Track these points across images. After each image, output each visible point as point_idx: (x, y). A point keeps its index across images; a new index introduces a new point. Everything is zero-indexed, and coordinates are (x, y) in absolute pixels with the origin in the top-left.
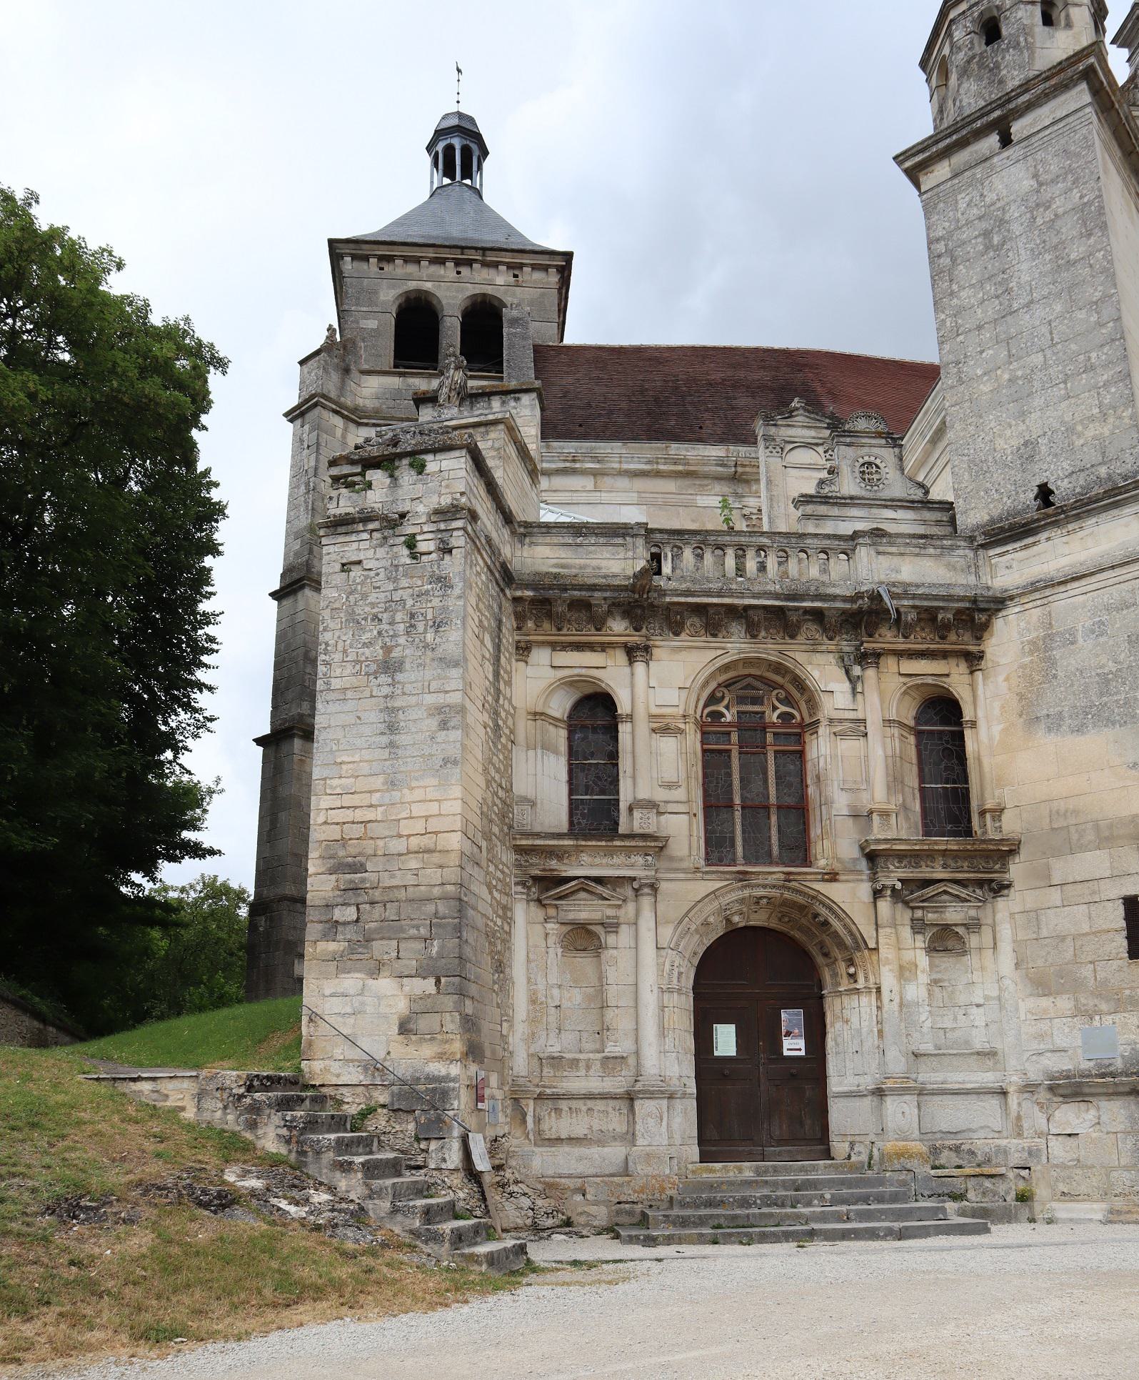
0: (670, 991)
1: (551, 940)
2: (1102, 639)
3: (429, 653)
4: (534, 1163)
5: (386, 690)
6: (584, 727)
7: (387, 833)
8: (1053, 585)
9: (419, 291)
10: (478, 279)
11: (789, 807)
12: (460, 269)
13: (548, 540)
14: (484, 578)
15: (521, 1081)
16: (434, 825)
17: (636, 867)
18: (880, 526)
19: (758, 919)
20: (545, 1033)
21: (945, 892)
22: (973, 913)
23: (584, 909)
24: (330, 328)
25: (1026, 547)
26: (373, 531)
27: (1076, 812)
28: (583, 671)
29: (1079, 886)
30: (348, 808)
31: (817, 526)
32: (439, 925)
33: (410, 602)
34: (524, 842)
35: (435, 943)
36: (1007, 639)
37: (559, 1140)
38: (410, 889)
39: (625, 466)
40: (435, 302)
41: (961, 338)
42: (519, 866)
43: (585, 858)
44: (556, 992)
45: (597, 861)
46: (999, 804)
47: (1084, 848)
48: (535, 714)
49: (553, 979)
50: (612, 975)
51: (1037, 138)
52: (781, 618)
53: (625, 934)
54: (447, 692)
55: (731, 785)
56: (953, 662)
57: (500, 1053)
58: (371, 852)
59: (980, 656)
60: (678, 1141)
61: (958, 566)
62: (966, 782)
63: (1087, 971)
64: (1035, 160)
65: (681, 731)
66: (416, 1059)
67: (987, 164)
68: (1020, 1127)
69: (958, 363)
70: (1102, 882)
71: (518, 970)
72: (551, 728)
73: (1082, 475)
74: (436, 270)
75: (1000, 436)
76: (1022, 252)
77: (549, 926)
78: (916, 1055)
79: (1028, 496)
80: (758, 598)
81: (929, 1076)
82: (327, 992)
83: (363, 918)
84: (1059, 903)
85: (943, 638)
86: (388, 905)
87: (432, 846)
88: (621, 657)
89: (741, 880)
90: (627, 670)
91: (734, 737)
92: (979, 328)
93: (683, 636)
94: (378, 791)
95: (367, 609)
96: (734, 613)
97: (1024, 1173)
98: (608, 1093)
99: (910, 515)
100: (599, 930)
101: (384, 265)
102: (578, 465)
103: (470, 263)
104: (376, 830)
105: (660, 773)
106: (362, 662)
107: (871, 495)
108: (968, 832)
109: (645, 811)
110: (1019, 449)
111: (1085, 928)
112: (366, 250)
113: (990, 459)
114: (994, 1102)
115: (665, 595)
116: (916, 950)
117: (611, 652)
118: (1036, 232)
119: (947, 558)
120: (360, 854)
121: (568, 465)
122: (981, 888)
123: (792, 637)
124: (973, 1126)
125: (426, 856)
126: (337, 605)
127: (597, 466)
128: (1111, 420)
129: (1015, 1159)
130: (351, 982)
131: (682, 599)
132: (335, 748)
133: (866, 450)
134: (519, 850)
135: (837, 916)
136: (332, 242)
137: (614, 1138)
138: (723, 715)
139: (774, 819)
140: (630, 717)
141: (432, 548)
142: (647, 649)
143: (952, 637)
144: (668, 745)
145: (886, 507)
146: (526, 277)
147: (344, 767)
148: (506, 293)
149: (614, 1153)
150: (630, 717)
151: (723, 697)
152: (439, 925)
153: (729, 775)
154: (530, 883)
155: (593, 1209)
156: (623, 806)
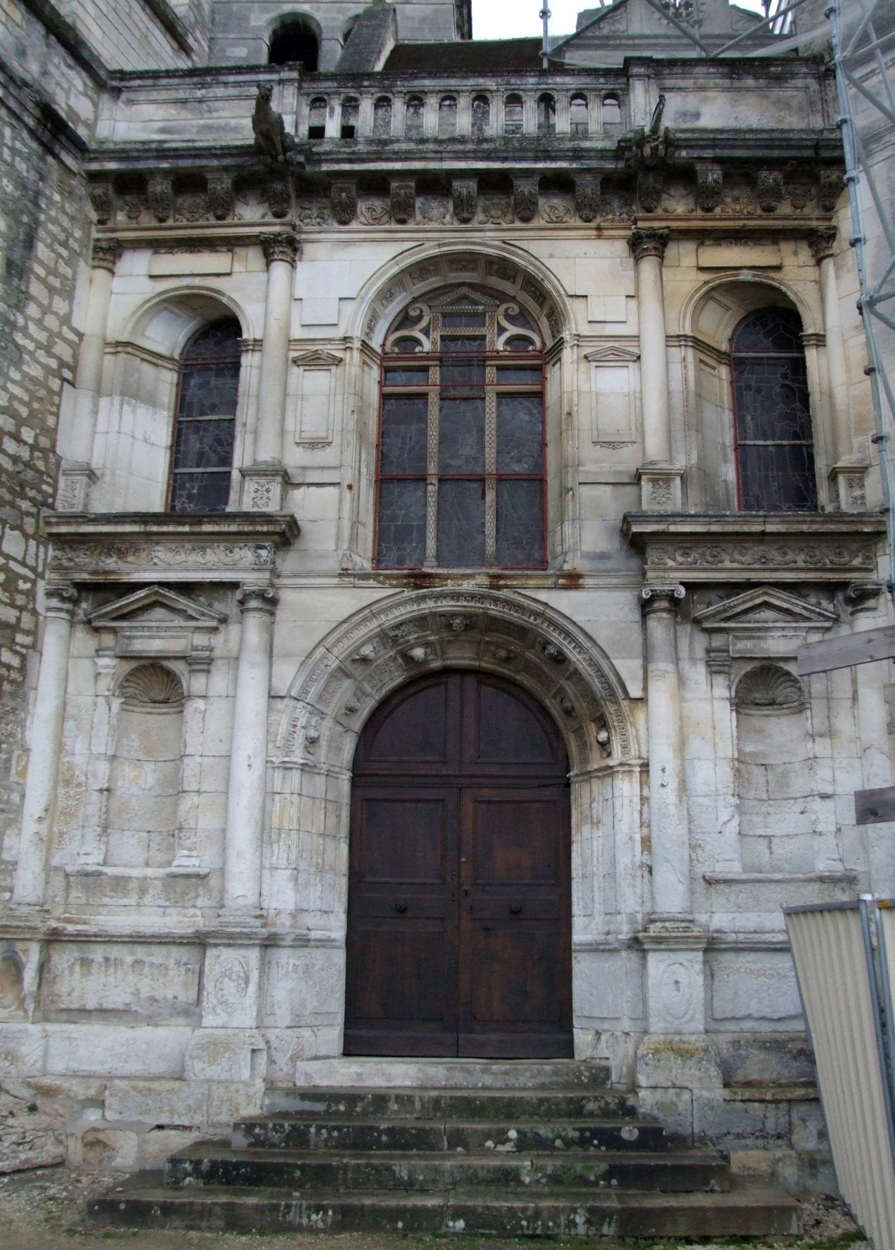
0: (286, 767)
1: (106, 683)
6: (205, 368)
13: (154, 95)
17: (242, 565)
20: (79, 833)
23: (157, 637)
28: (197, 281)
34: (64, 529)
40: (314, 26)
43: (161, 553)
45: (181, 558)
46: (863, 460)
48: (118, 344)
49: (100, 747)
55: (425, 447)
56: (787, 247)
59: (831, 235)
60: (283, 1017)
61: (794, 103)
62: (810, 436)
78: (709, 882)
85: (768, 209)
89: (417, 587)
90: (263, 276)
91: (435, 374)
93: (354, 225)
96: (434, 185)
98: (167, 935)
100: (177, 667)
105: (308, 426)
109: (263, 481)
115: (320, 162)
116: (710, 701)
117: (240, 251)
122: (831, 599)
131: (346, 167)
135: (579, 646)
138: (418, 342)
139: (490, 496)
144: (316, 382)
149: (166, 1039)
151: (420, 318)
153: (423, 433)
154: (73, 592)
156: (235, 475)
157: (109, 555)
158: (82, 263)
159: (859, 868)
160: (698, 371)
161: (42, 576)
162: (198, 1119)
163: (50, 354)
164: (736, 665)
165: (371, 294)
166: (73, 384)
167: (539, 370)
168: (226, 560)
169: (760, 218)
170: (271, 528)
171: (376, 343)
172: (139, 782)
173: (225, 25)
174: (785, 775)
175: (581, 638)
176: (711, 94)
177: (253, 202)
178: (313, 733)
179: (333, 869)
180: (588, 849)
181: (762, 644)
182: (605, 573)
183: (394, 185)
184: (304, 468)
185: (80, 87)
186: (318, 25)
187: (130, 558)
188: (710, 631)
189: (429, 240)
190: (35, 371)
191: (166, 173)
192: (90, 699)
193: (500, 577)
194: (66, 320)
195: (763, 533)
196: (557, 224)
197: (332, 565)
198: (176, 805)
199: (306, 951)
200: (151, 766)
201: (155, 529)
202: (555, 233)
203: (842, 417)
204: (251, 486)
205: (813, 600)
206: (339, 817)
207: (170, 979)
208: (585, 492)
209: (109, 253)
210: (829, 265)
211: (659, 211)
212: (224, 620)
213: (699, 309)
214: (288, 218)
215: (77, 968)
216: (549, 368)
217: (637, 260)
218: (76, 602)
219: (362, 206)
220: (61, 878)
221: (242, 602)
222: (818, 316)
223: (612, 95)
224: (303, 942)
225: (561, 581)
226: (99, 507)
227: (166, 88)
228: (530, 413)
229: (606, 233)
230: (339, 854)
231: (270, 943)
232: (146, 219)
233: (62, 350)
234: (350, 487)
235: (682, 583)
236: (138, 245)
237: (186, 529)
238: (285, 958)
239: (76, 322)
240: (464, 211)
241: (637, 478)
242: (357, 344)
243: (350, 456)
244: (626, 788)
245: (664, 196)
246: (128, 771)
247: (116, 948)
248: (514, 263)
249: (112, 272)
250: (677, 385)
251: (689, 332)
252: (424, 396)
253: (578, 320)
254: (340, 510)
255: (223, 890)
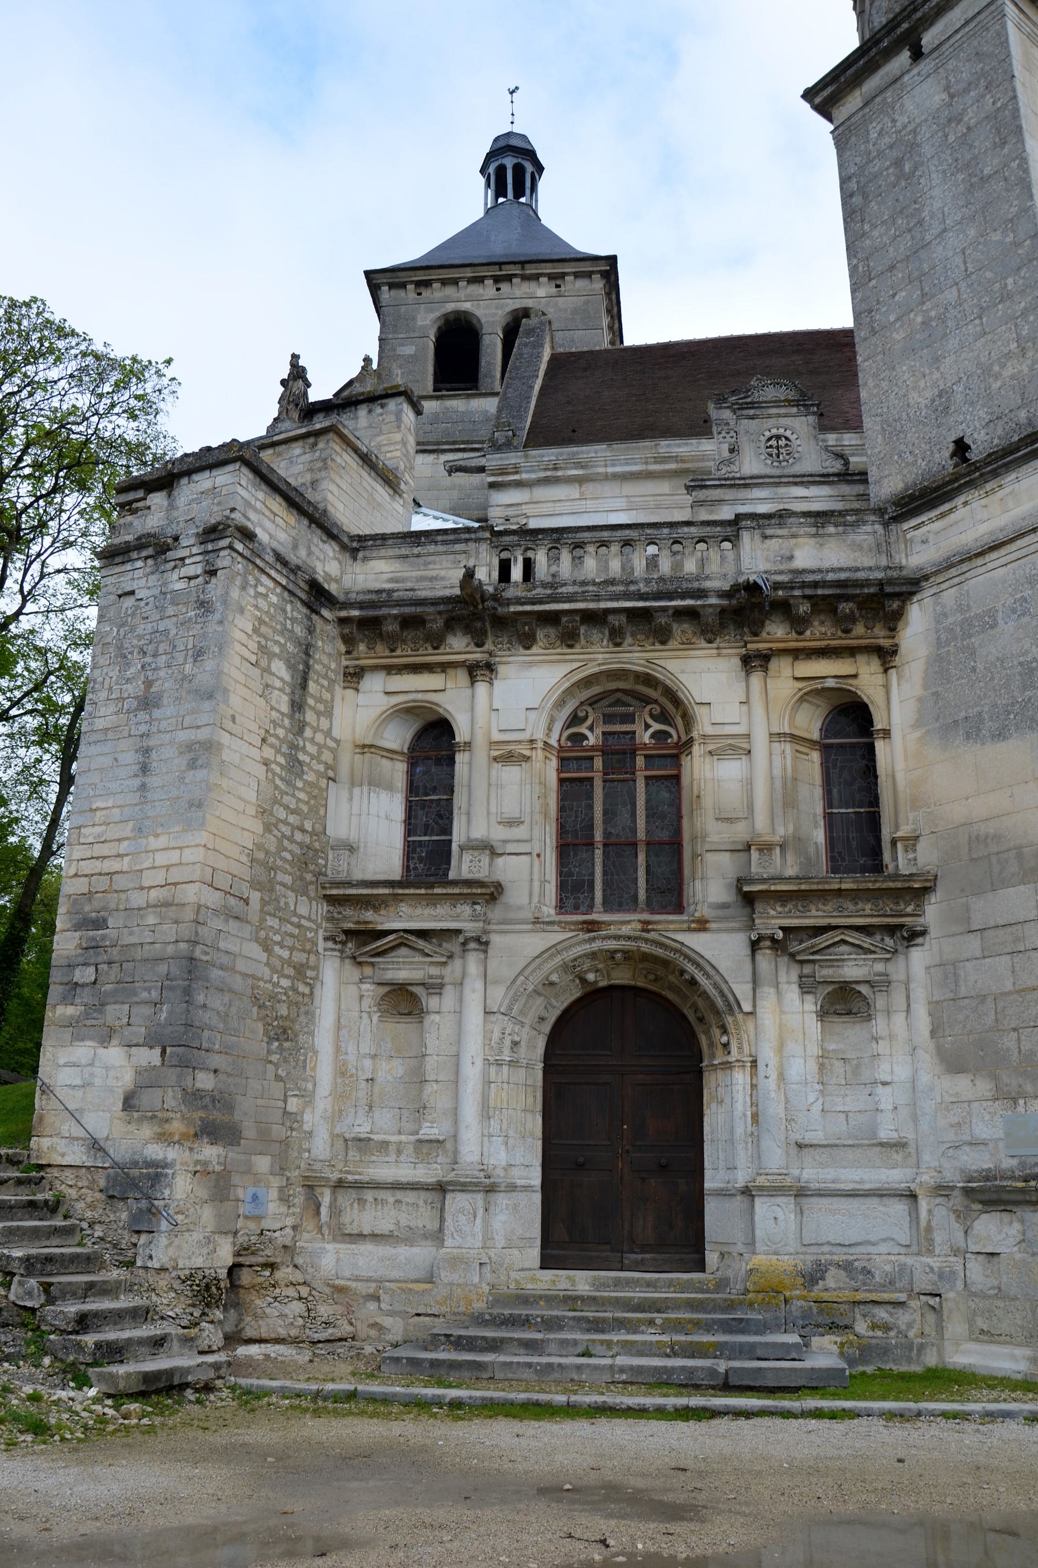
0: (499, 1064)
1: (366, 1003)
2: (1025, 620)
3: (186, 685)
4: (324, 1262)
5: (143, 728)
7: (131, 885)
8: (970, 559)
9: (466, 313)
10: (518, 293)
11: (661, 843)
12: (500, 286)
13: (383, 552)
14: (274, 599)
15: (317, 1166)
16: (175, 876)
17: (459, 917)
18: (787, 506)
19: (622, 977)
20: (353, 1110)
21: (844, 942)
22: (879, 967)
23: (404, 968)
24: (367, 360)
25: (943, 515)
26: (146, 558)
27: (997, 837)
28: (420, 696)
29: (1001, 932)
30: (97, 858)
31: (711, 512)
32: (171, 988)
33: (173, 632)
34: (334, 892)
35: (165, 1008)
36: (918, 625)
37: (361, 1236)
38: (146, 947)
39: (610, 470)
40: (475, 321)
41: (873, 282)
42: (330, 919)
43: (404, 908)
44: (368, 1063)
45: (419, 911)
46: (915, 830)
47: (1005, 883)
48: (364, 746)
49: (365, 1049)
50: (432, 1043)
51: (947, 46)
52: (650, 618)
53: (449, 997)
54: (198, 727)
55: (592, 818)
56: (861, 659)
57: (278, 1131)
58: (113, 906)
59: (894, 651)
60: (500, 1241)
61: (865, 545)
63: (1009, 1041)
64: (947, 70)
65: (527, 759)
66: (134, 1142)
67: (898, 85)
68: (931, 1241)
69: (870, 311)
70: (1027, 926)
71: (323, 1038)
72: (385, 762)
73: (1000, 423)
74: (475, 289)
75: (914, 389)
76: (934, 176)
77: (364, 987)
78: (800, 1146)
79: (943, 456)
80: (618, 600)
81: (811, 1172)
82: (62, 1061)
83: (101, 979)
84: (978, 954)
85: (847, 631)
86: (124, 965)
87: (170, 899)
88: (461, 677)
89: (589, 931)
90: (469, 691)
91: (598, 763)
92: (892, 268)
93: (535, 650)
94: (127, 839)
95: (135, 642)
96: (593, 618)
97: (933, 1301)
98: (418, 1183)
99: (824, 491)
100: (418, 990)
101: (422, 290)
102: (560, 473)
103: (509, 278)
104: (121, 882)
105: (506, 811)
106: (124, 699)
107: (777, 472)
108: (878, 867)
109: (476, 853)
110: (933, 401)
111: (1008, 986)
112: (403, 277)
113: (904, 417)
114: (900, 1208)
115: (508, 605)
117: (451, 672)
118: (949, 152)
119: (851, 537)
120: (105, 909)
121: (549, 473)
122: (892, 936)
123: (663, 643)
124: (873, 1238)
125: (163, 909)
126: (109, 640)
127: (580, 472)
128: (1030, 354)
129: (923, 1283)
130: (83, 1051)
131: (528, 608)
132: (92, 793)
133: (772, 422)
134: (332, 900)
136: (368, 274)
137: (425, 1237)
139: (641, 858)
140: (468, 745)
141: (199, 571)
142: (490, 667)
143: (859, 629)
144: (511, 774)
145: (796, 484)
146: (569, 287)
147: (98, 814)
148: (547, 304)
149: (416, 1256)
150: (468, 745)
151: (586, 717)
152: (171, 988)
153: (591, 807)
154: (343, 937)
155: (387, 1321)
156: (455, 847)
157: (366, 909)
158: (337, 687)
159: (910, 1136)
160: (795, 759)
161: (319, 926)
162: (444, 1309)
163: (320, 762)
164: (820, 987)
165: (549, 705)
166: (334, 781)
167: (676, 757)
168: (452, 913)
169: (840, 638)
170: (484, 891)
171: (553, 742)
172: (391, 1071)
173: (395, 326)
174: (858, 1066)
175: (708, 968)
176: (800, 540)
177: (459, 634)
178: (517, 1039)
179: (532, 1135)
180: (715, 1120)
181: (840, 971)
182: (726, 919)
183: (564, 619)
184: (505, 842)
185: (331, 554)
186: (479, 321)
187: (382, 912)
188: (802, 962)
189: (591, 660)
190: (310, 777)
191: (396, 617)
192: (356, 1014)
193: (648, 923)
194: (328, 733)
195: (840, 890)
196: (688, 644)
197: (529, 915)
198: (421, 1091)
199: (514, 1194)
200: (401, 1061)
201: (400, 891)
202: (686, 653)
203: (901, 796)
204: (467, 857)
205: (878, 937)
206: (535, 1097)
207: (418, 1213)
208: (710, 858)
209: (354, 676)
210: (893, 672)
211: (764, 634)
212: (450, 957)
213: (795, 709)
214: (486, 647)
215: (356, 1205)
216: (683, 757)
217: (748, 673)
218: (344, 943)
219: (540, 634)
220: (341, 1141)
221: (464, 944)
222: (885, 714)
223: (726, 539)
224: (512, 1188)
225: (693, 925)
226: (358, 876)
227: (392, 547)
228: (670, 792)
229: (724, 651)
230: (535, 1124)
231: (491, 1189)
232: (381, 649)
233: (327, 756)
234: (538, 856)
235: (781, 928)
236: (375, 668)
237: (423, 891)
238: (502, 1200)
239: (336, 733)
240: (616, 637)
241: (748, 848)
242: (540, 744)
243: (537, 832)
244: (740, 1078)
245: (768, 622)
246: (384, 1065)
247: (382, 1192)
248: (656, 678)
249: (357, 690)
250: (777, 772)
251: (787, 730)
252: (591, 779)
253: (704, 723)
254: (531, 873)
255: (456, 1152)
